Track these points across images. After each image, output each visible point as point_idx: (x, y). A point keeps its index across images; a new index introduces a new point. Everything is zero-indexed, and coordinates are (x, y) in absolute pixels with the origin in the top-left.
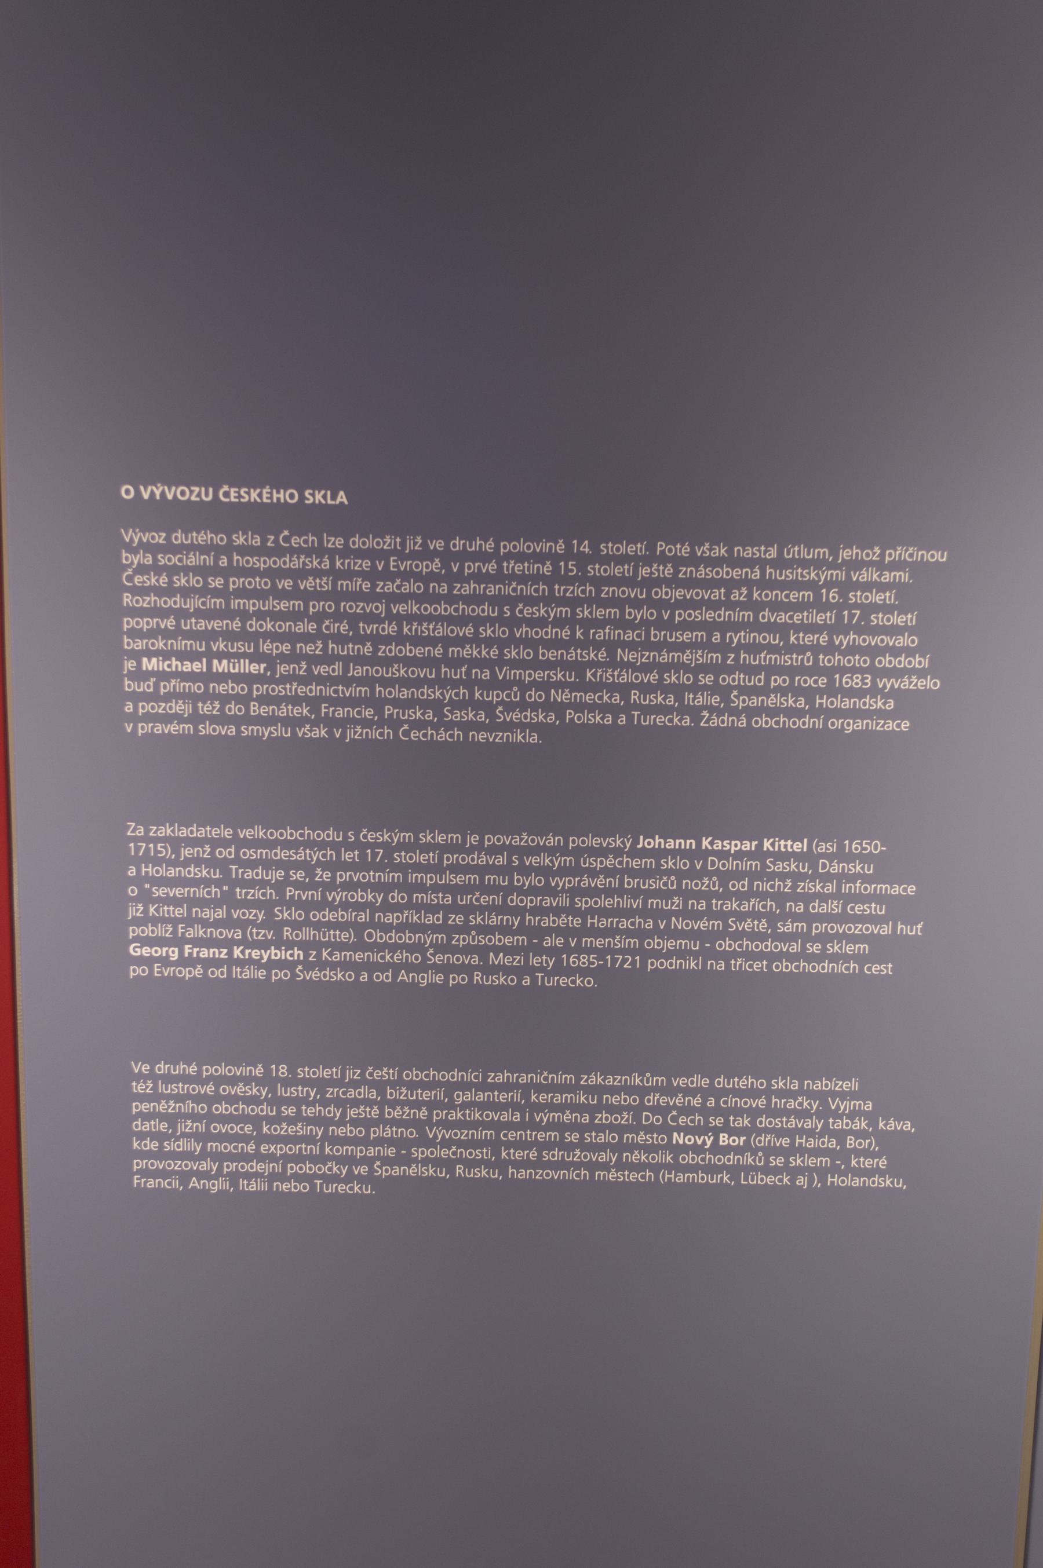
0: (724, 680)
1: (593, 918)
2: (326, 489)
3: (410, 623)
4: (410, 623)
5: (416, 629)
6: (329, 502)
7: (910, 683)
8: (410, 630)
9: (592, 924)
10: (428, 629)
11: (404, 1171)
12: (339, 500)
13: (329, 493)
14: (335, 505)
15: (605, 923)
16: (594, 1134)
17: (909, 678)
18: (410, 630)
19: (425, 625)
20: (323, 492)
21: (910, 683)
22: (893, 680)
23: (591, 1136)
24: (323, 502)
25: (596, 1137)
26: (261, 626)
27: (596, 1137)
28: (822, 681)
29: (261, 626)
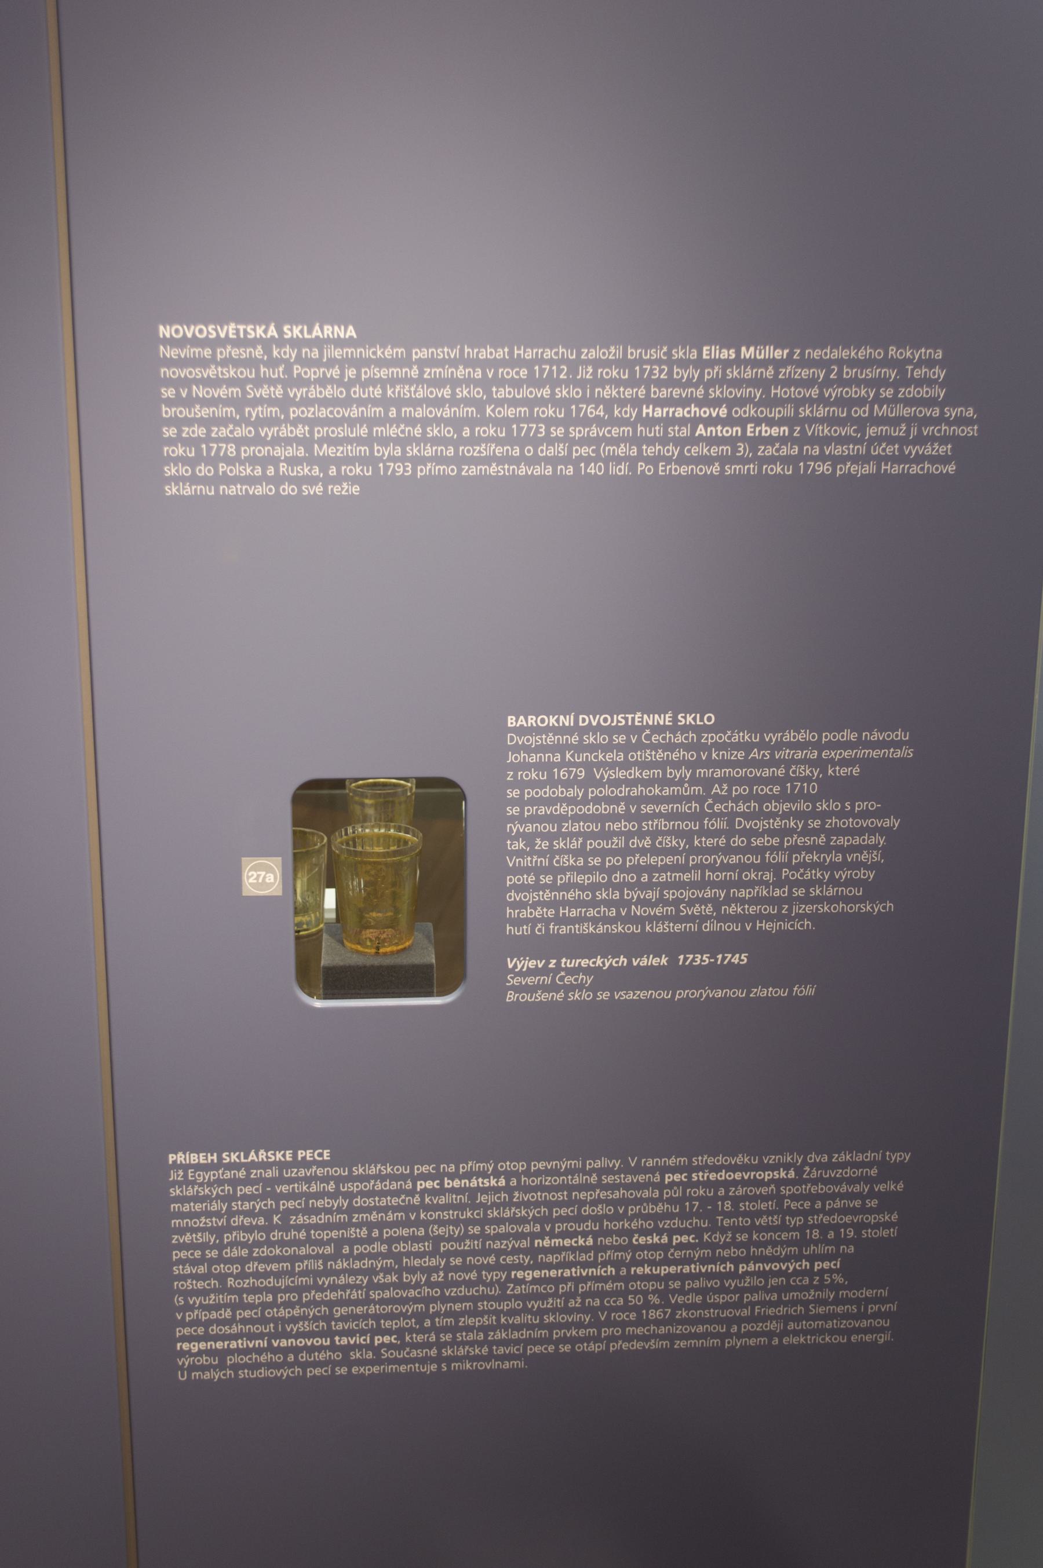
0: (736, 412)
1: (564, 909)
2: (303, 324)
3: (393, 386)
4: (393, 386)
5: (399, 392)
6: (306, 336)
7: (933, 449)
8: (394, 393)
9: (564, 914)
10: (410, 392)
11: (406, 372)
12: (314, 334)
13: (305, 328)
14: (312, 339)
15: (574, 913)
16: (677, 428)
17: (932, 445)
18: (394, 393)
19: (407, 387)
20: (300, 327)
21: (933, 449)
22: (917, 447)
23: (674, 431)
24: (300, 336)
25: (679, 431)
26: (271, 1252)
27: (679, 431)
28: (633, 1316)
29: (271, 1252)
